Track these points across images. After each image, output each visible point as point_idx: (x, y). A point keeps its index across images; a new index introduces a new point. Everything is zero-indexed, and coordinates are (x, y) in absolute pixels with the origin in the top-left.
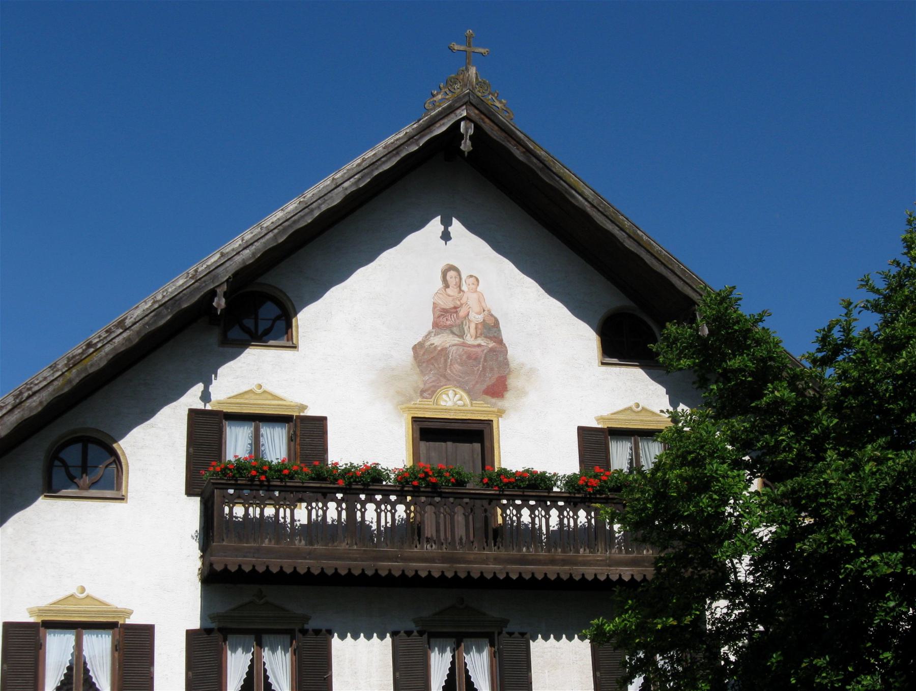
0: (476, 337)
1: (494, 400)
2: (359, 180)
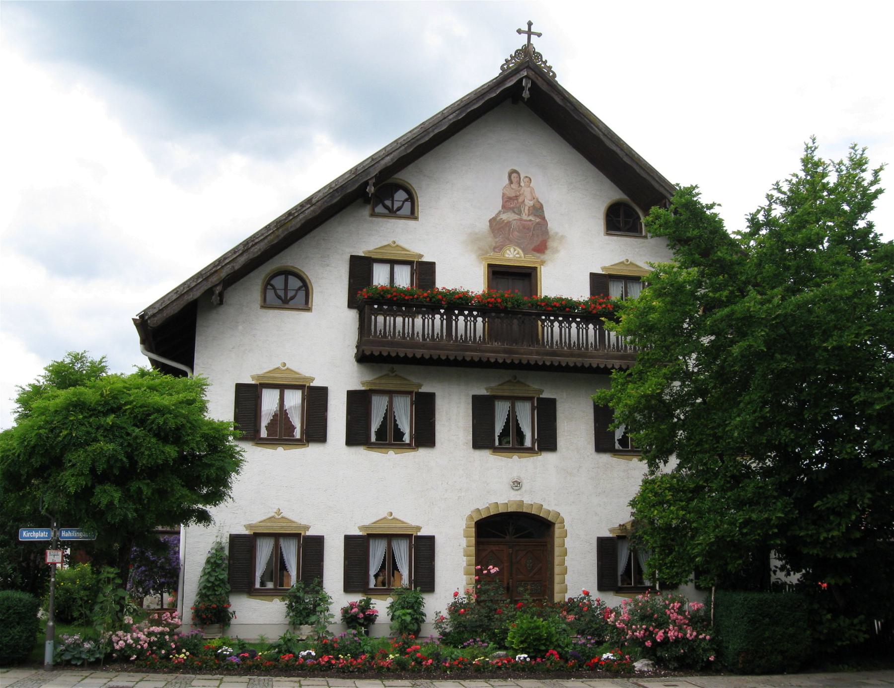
0: (529, 215)
1: (538, 255)
2: (458, 115)
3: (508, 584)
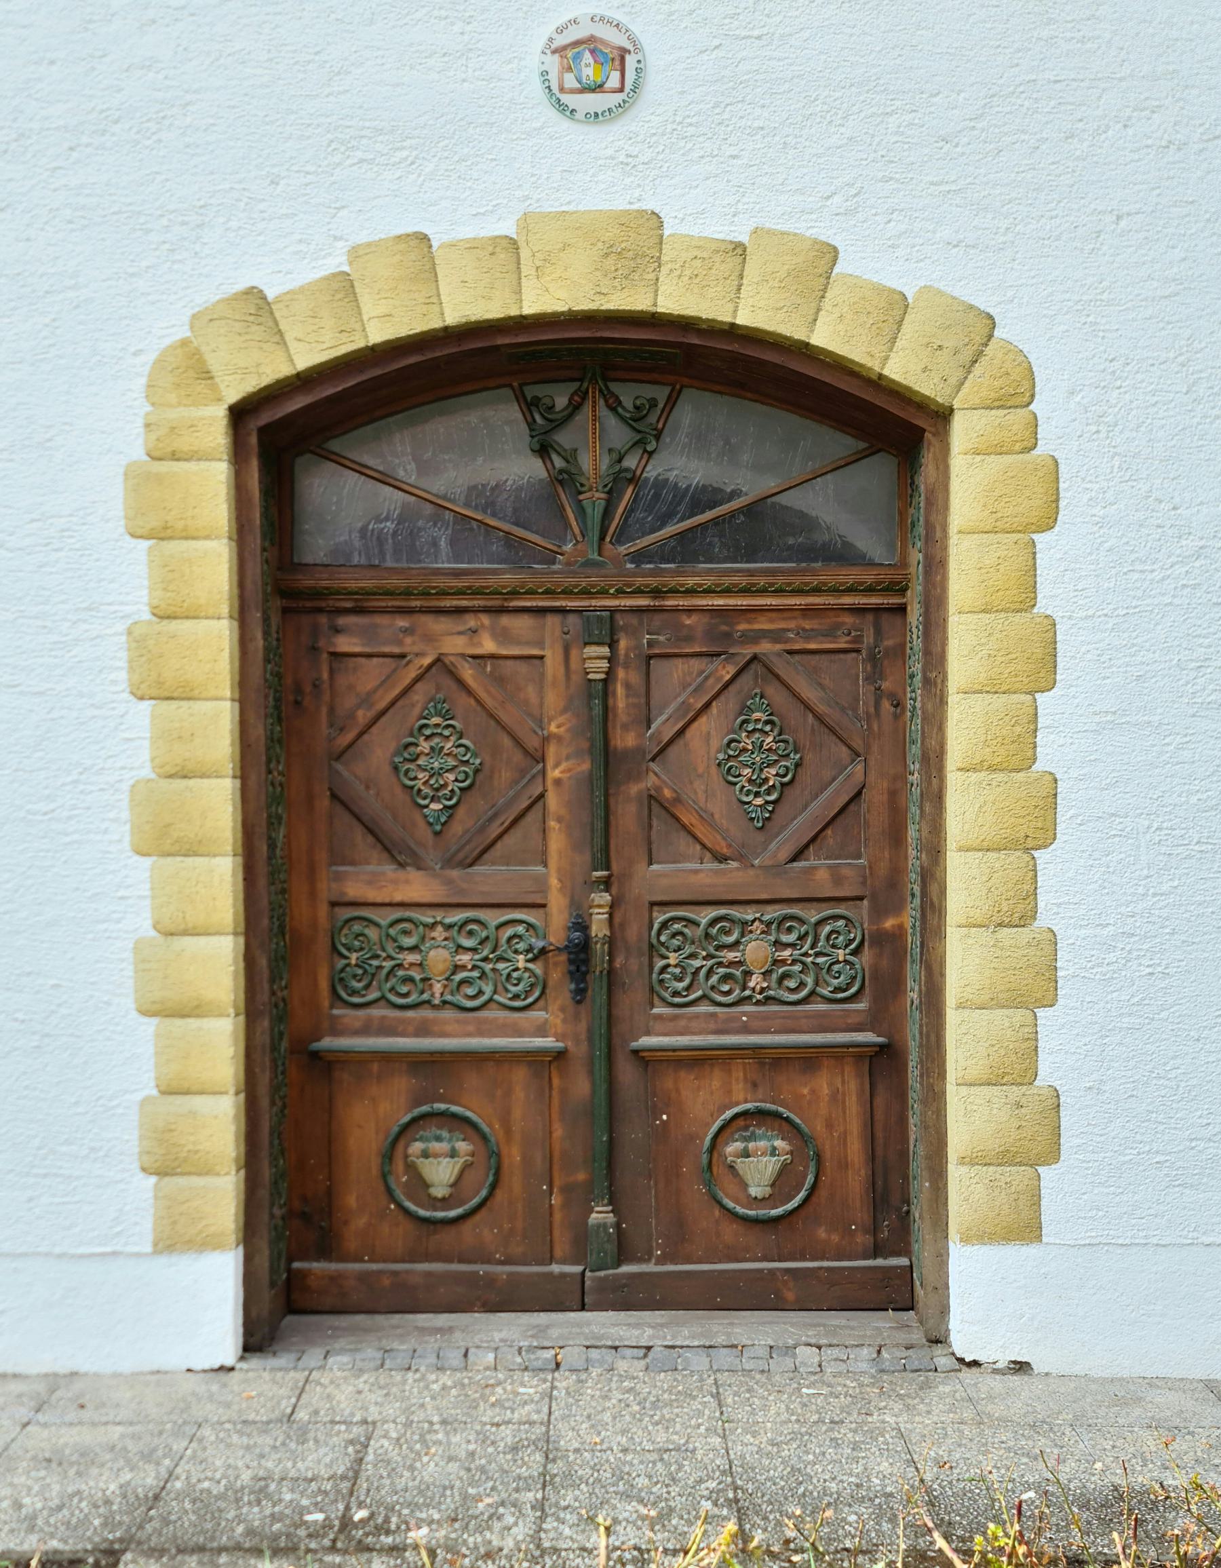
3: (581, 926)
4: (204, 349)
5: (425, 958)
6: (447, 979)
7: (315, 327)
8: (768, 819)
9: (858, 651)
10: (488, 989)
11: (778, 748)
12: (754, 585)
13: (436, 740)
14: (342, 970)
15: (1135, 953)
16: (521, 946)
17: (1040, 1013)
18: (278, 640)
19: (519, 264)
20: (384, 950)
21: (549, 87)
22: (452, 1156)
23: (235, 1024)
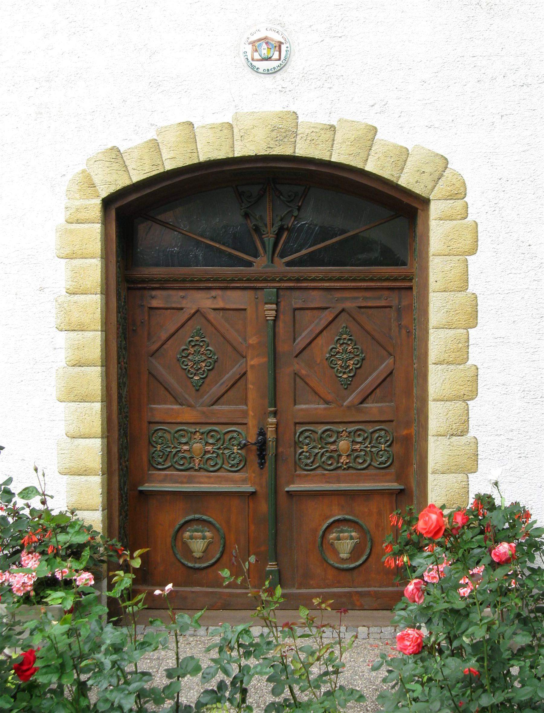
3: (262, 433)
4: (92, 174)
5: (191, 448)
6: (201, 458)
7: (141, 164)
8: (349, 384)
9: (390, 307)
10: (220, 462)
11: (354, 352)
12: (342, 277)
13: (197, 347)
14: (154, 453)
15: (513, 448)
16: (235, 442)
17: (470, 475)
18: (125, 302)
19: (233, 135)
20: (172, 444)
21: (247, 58)
22: (203, 539)
23: (102, 479)
